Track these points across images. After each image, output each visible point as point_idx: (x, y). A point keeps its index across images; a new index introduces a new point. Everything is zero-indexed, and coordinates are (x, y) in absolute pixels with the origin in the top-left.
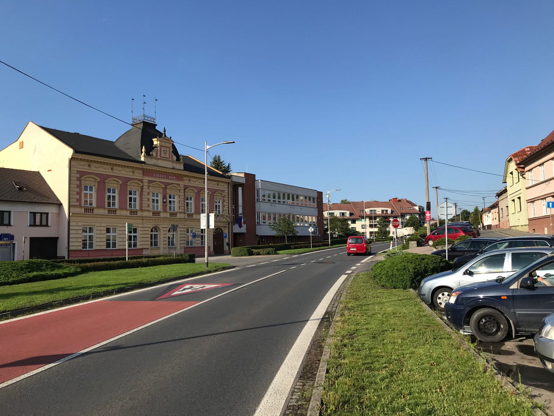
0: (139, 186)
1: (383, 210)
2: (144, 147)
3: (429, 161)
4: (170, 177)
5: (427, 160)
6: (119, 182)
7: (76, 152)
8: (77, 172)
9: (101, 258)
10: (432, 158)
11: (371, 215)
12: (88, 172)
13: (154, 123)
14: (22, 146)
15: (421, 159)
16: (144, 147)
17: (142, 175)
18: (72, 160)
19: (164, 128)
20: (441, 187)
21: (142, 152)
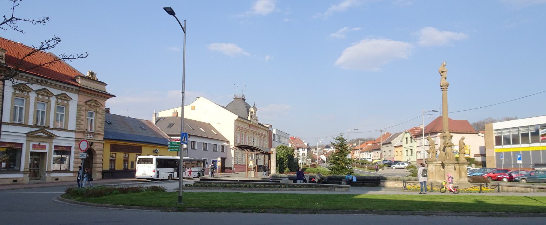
7: (239, 117)
18: (236, 121)
21: (248, 115)
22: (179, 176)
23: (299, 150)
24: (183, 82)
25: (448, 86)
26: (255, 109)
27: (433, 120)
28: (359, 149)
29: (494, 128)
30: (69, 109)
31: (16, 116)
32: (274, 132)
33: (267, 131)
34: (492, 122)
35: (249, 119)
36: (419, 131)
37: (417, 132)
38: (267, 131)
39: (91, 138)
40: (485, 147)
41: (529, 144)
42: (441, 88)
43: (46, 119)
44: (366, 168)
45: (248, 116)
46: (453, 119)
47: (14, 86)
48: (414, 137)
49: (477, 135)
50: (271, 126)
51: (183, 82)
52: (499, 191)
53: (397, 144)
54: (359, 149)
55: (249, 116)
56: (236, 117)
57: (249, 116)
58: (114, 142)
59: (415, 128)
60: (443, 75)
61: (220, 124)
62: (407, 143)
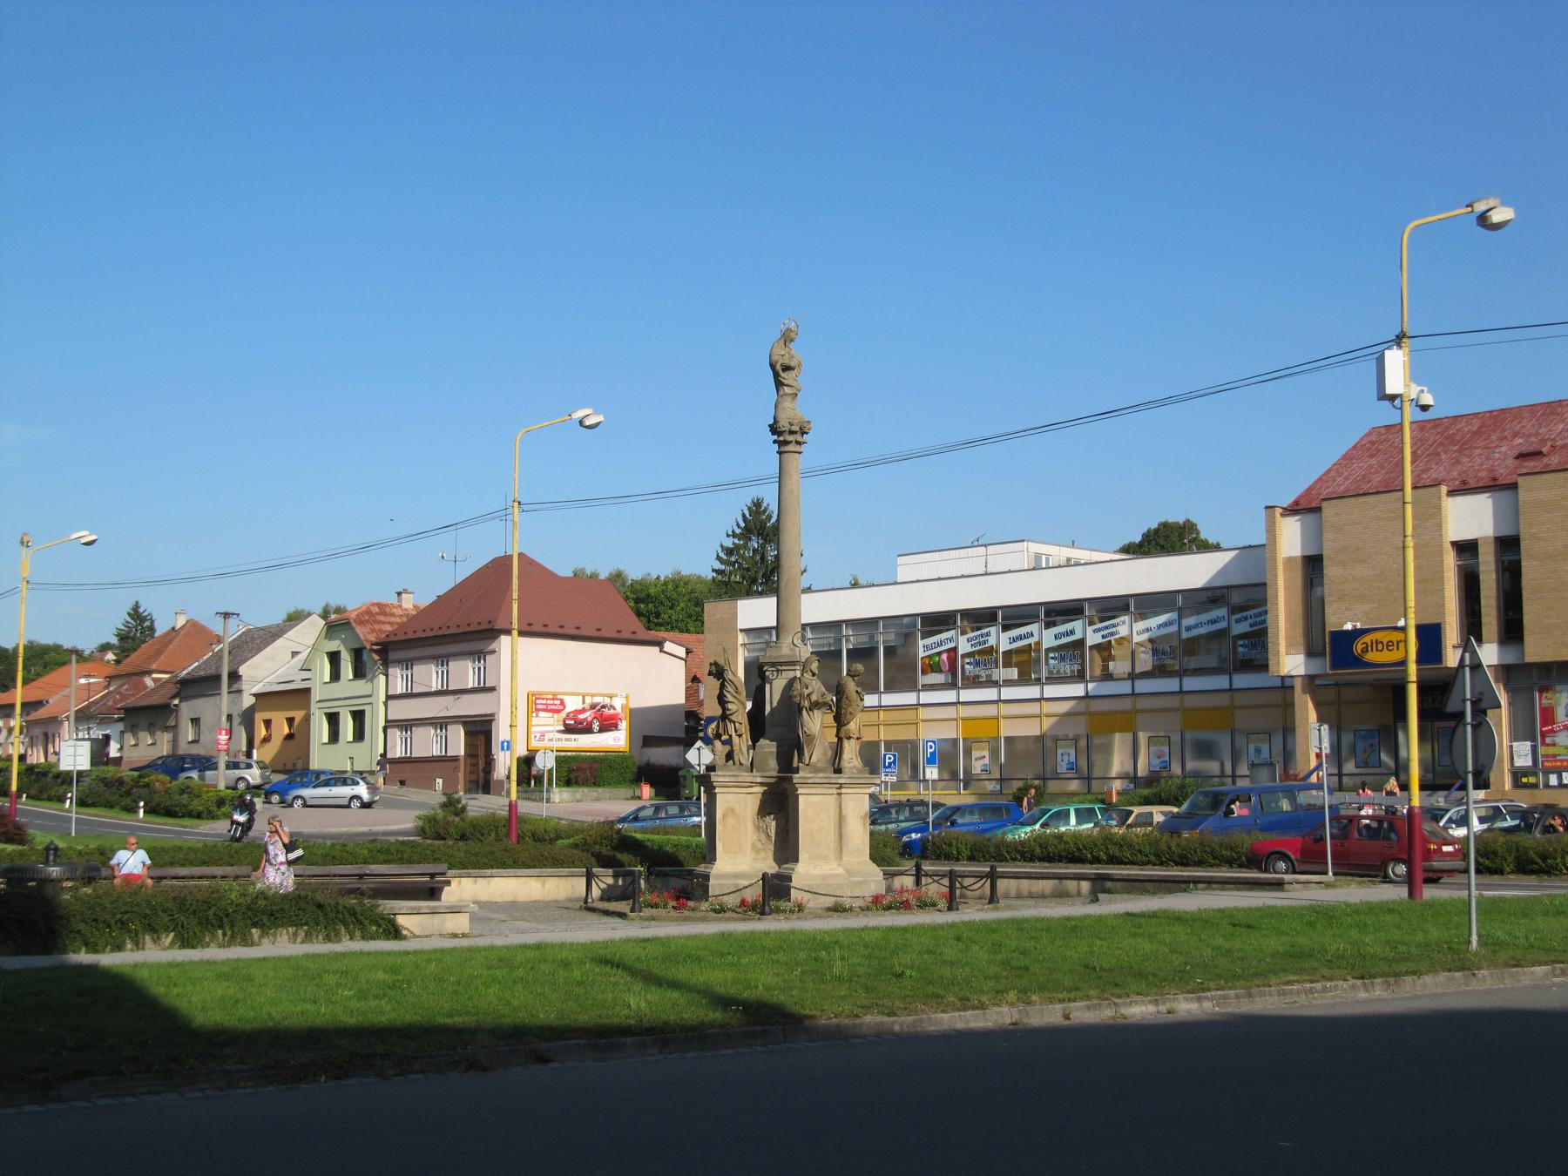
25: (803, 433)
27: (460, 579)
29: (742, 624)
31: (1298, 609)
34: (777, 596)
36: (398, 620)
37: (388, 628)
39: (1013, 883)
41: (876, 696)
43: (1395, 671)
44: (142, 811)
46: (560, 575)
48: (375, 651)
49: (658, 649)
52: (993, 898)
53: (270, 684)
59: (379, 605)
60: (785, 382)
62: (335, 676)
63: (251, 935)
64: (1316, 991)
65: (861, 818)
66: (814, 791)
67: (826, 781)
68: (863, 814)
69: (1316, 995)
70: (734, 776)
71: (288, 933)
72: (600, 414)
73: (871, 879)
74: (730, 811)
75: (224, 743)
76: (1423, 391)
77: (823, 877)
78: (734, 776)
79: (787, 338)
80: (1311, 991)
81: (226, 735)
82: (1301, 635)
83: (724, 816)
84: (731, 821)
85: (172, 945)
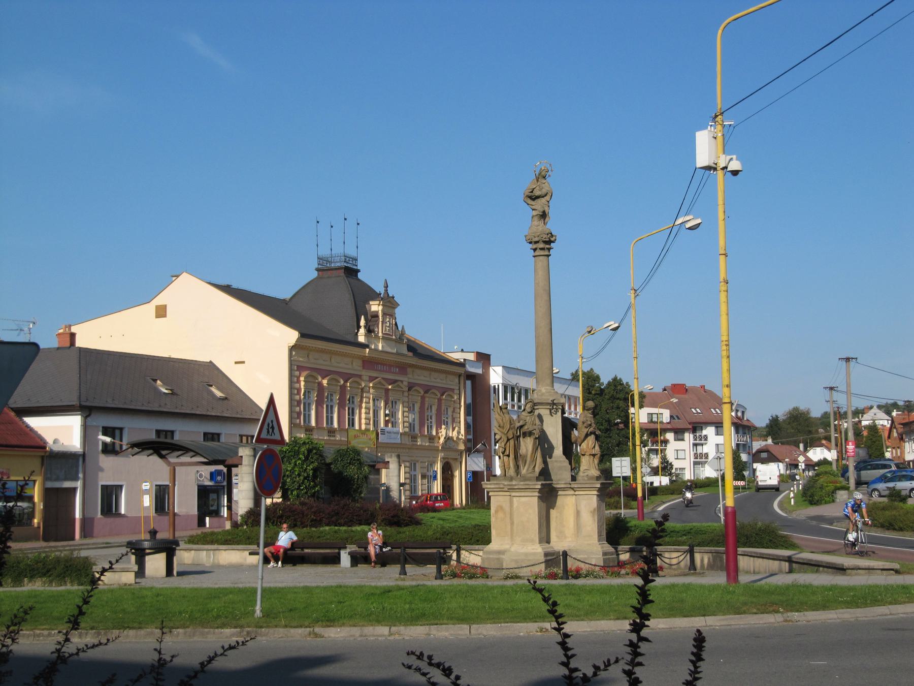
0: (435, 398)
1: (652, 414)
2: (363, 317)
3: (852, 363)
4: (392, 368)
5: (849, 361)
6: (402, 388)
7: (303, 335)
8: (369, 378)
9: (768, 490)
10: (857, 358)
11: (652, 426)
12: (330, 371)
13: (355, 268)
14: (161, 312)
15: (839, 359)
16: (363, 317)
17: (361, 368)
18: (292, 349)
19: (386, 280)
20: (839, 389)
21: (359, 327)
22: (199, 528)
23: (704, 432)
24: (872, 15)
26: (390, 303)
28: (850, 415)
30: (203, 362)
32: (496, 377)
33: (460, 376)
35: (361, 339)
38: (460, 376)
40: (503, 367)
42: (534, 256)
45: (358, 331)
47: (611, 576)
50: (484, 359)
51: (872, 15)
54: (850, 415)
55: (362, 331)
56: (292, 336)
57: (362, 331)
58: (250, 551)
61: (236, 363)
63: (24, 582)
64: (43, 635)
65: (591, 512)
66: (523, 494)
67: (527, 487)
68: (592, 509)
69: (41, 638)
70: (497, 484)
71: (42, 580)
72: (698, 218)
73: (594, 556)
74: (500, 508)
75: (851, 451)
76: (731, 159)
77: (526, 554)
78: (497, 484)
79: (542, 176)
80: (39, 636)
81: (852, 445)
82: (526, 378)
83: (496, 512)
84: (501, 515)
85: (47, 586)
